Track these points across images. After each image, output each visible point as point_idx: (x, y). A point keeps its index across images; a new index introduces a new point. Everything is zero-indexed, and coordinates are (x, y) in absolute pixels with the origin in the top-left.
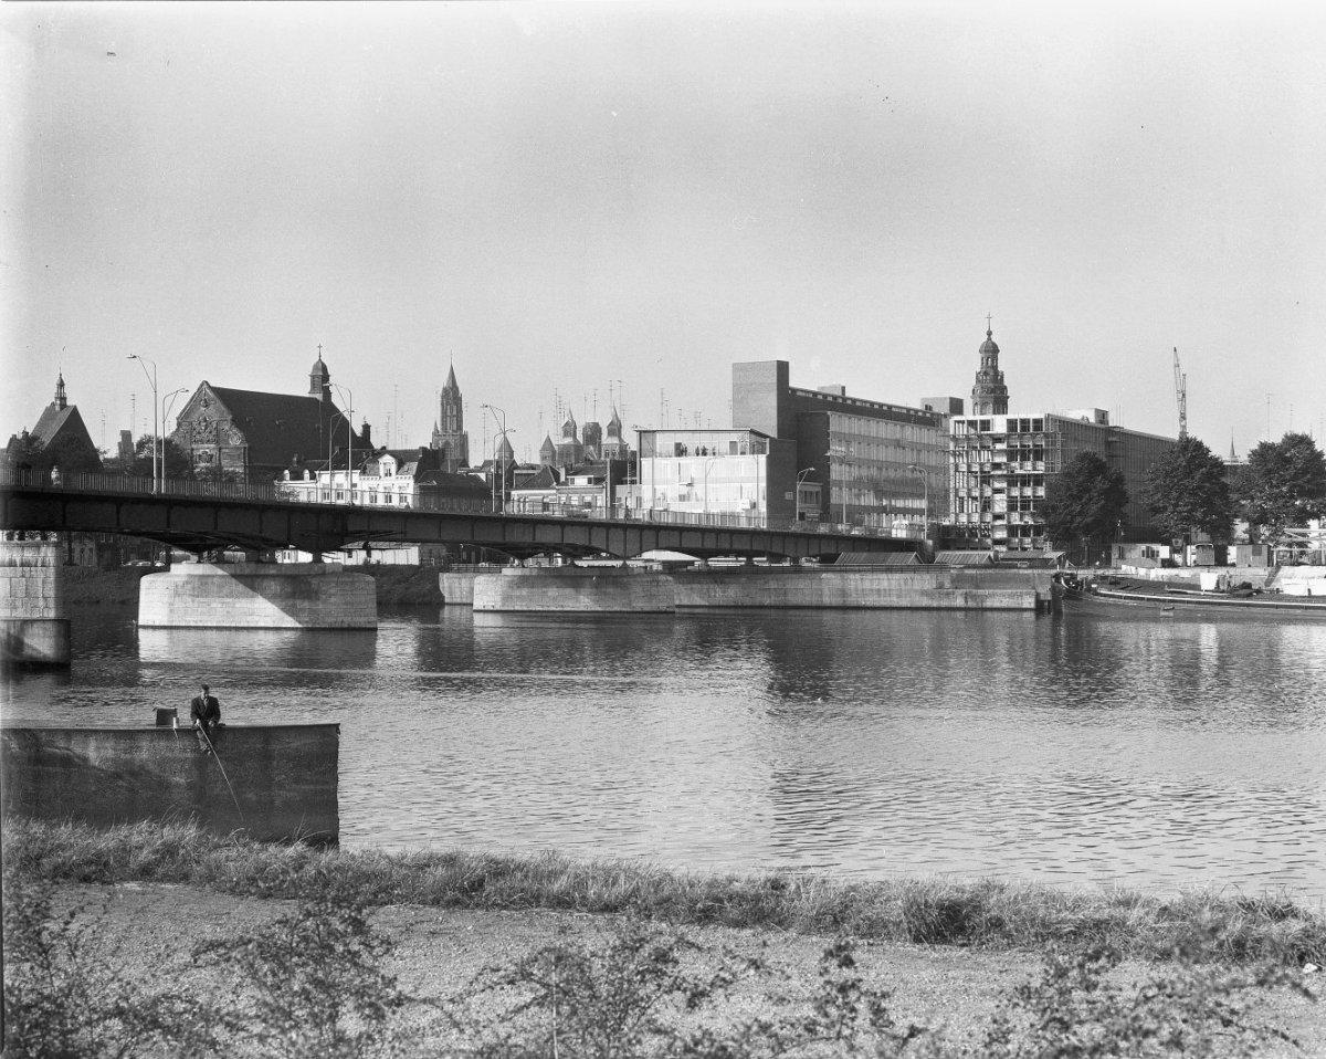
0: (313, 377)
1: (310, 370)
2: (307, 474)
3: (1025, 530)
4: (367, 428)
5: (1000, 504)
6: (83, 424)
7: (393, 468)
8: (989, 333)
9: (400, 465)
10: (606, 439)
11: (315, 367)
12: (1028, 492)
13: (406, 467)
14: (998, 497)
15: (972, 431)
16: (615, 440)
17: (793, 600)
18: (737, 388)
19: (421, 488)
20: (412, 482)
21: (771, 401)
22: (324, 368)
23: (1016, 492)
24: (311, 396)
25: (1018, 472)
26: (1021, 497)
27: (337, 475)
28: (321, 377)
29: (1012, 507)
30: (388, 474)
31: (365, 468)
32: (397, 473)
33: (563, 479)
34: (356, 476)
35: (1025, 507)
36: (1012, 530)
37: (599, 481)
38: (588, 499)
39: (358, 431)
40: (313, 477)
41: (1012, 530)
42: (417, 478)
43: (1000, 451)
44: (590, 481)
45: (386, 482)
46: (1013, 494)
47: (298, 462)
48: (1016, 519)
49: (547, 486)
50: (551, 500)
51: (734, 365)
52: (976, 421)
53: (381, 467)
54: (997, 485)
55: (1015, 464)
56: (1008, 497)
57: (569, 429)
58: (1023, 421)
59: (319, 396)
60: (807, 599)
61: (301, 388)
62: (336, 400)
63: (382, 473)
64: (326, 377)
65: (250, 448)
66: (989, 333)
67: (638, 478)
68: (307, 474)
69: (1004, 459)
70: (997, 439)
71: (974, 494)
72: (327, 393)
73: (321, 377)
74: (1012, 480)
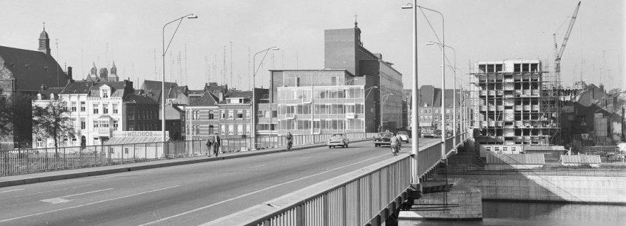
0: (41, 40)
1: (38, 37)
2: (52, 96)
3: (526, 132)
4: (70, 69)
5: (509, 115)
6: (11, 49)
7: (109, 93)
8: (356, 24)
9: (113, 91)
10: (109, 75)
11: (42, 35)
12: (528, 108)
13: (116, 92)
14: (508, 111)
15: (482, 72)
16: (114, 76)
17: (502, 194)
18: (327, 45)
19: (127, 105)
20: (121, 101)
21: (351, 52)
22: (47, 35)
23: (520, 108)
24: (40, 51)
25: (522, 96)
26: (524, 111)
27: (81, 97)
28: (45, 40)
29: (517, 117)
30: (106, 96)
31: (90, 93)
32: (111, 95)
33: (221, 99)
34: (84, 97)
35: (526, 117)
36: (517, 132)
37: (246, 101)
38: (240, 112)
39: (65, 70)
40: (56, 98)
41: (517, 132)
42: (124, 99)
43: (509, 83)
44: (241, 101)
45: (105, 101)
46: (492, 110)
47: (44, 88)
48: (520, 125)
49: (212, 104)
50: (215, 112)
51: (326, 31)
52: (493, 65)
53: (101, 92)
54: (508, 104)
55: (520, 92)
56: (516, 111)
57: (94, 71)
58: (524, 65)
59: (44, 51)
60: (516, 194)
61: (34, 46)
62: (53, 54)
63: (101, 95)
64: (48, 41)
65: (16, 81)
66: (356, 24)
67: (270, 99)
68: (52, 96)
69: (512, 88)
70: (507, 76)
71: (484, 110)
72: (49, 50)
73: (45, 40)
74: (518, 101)
